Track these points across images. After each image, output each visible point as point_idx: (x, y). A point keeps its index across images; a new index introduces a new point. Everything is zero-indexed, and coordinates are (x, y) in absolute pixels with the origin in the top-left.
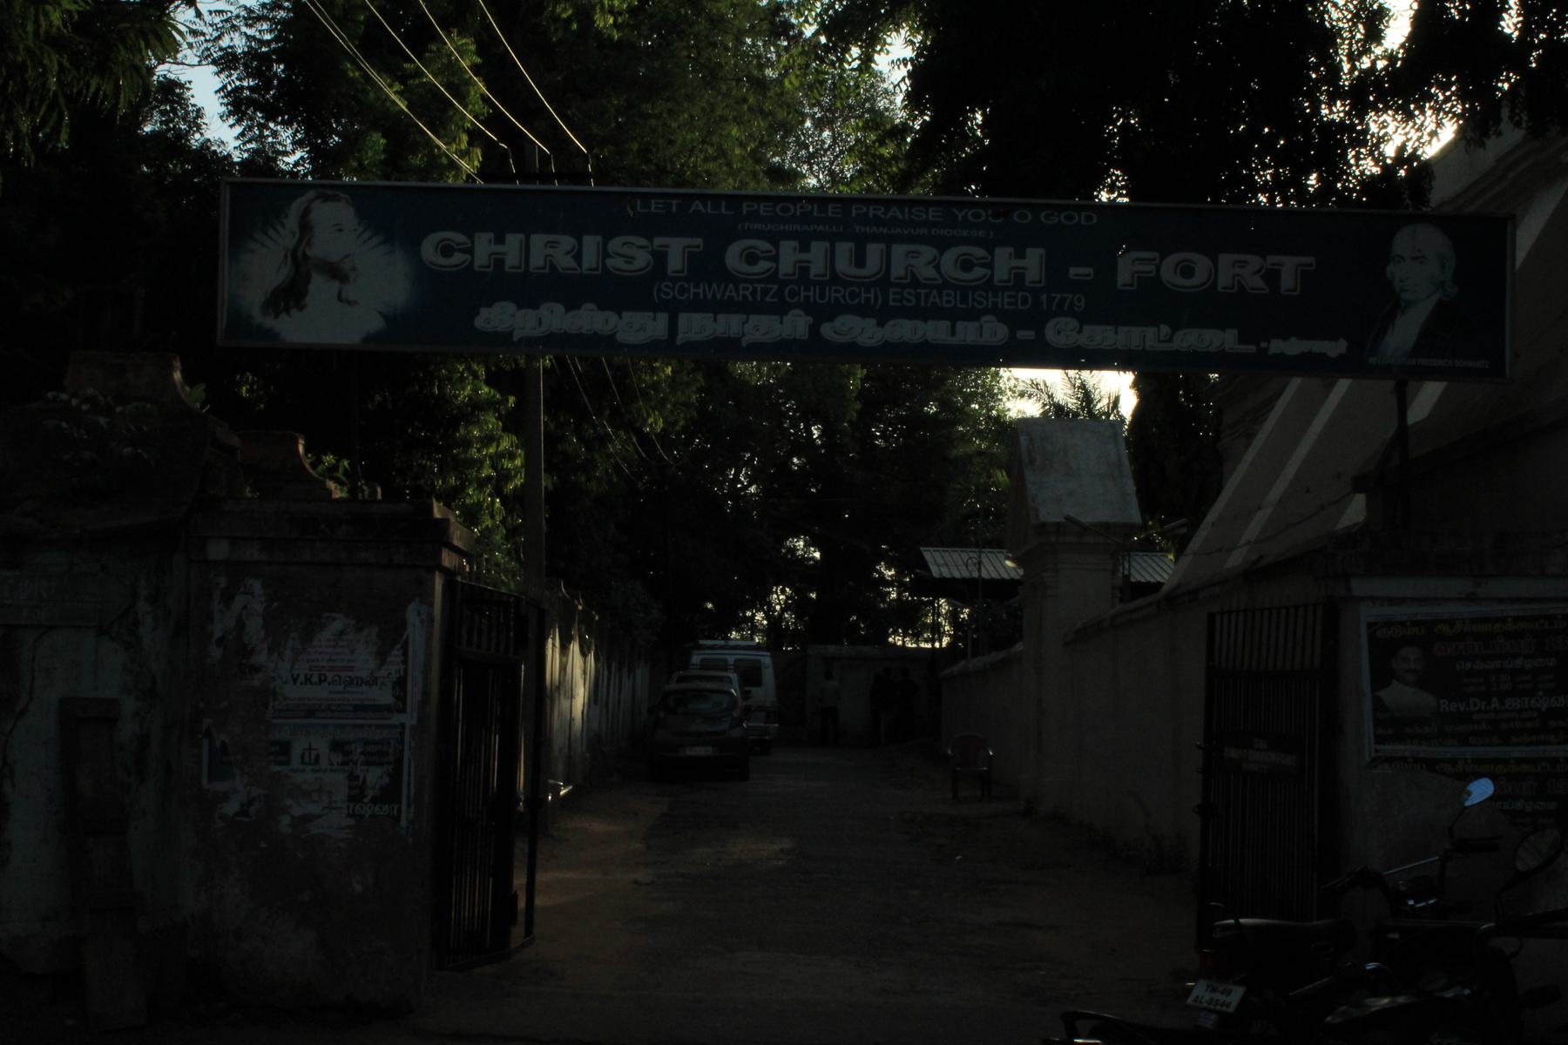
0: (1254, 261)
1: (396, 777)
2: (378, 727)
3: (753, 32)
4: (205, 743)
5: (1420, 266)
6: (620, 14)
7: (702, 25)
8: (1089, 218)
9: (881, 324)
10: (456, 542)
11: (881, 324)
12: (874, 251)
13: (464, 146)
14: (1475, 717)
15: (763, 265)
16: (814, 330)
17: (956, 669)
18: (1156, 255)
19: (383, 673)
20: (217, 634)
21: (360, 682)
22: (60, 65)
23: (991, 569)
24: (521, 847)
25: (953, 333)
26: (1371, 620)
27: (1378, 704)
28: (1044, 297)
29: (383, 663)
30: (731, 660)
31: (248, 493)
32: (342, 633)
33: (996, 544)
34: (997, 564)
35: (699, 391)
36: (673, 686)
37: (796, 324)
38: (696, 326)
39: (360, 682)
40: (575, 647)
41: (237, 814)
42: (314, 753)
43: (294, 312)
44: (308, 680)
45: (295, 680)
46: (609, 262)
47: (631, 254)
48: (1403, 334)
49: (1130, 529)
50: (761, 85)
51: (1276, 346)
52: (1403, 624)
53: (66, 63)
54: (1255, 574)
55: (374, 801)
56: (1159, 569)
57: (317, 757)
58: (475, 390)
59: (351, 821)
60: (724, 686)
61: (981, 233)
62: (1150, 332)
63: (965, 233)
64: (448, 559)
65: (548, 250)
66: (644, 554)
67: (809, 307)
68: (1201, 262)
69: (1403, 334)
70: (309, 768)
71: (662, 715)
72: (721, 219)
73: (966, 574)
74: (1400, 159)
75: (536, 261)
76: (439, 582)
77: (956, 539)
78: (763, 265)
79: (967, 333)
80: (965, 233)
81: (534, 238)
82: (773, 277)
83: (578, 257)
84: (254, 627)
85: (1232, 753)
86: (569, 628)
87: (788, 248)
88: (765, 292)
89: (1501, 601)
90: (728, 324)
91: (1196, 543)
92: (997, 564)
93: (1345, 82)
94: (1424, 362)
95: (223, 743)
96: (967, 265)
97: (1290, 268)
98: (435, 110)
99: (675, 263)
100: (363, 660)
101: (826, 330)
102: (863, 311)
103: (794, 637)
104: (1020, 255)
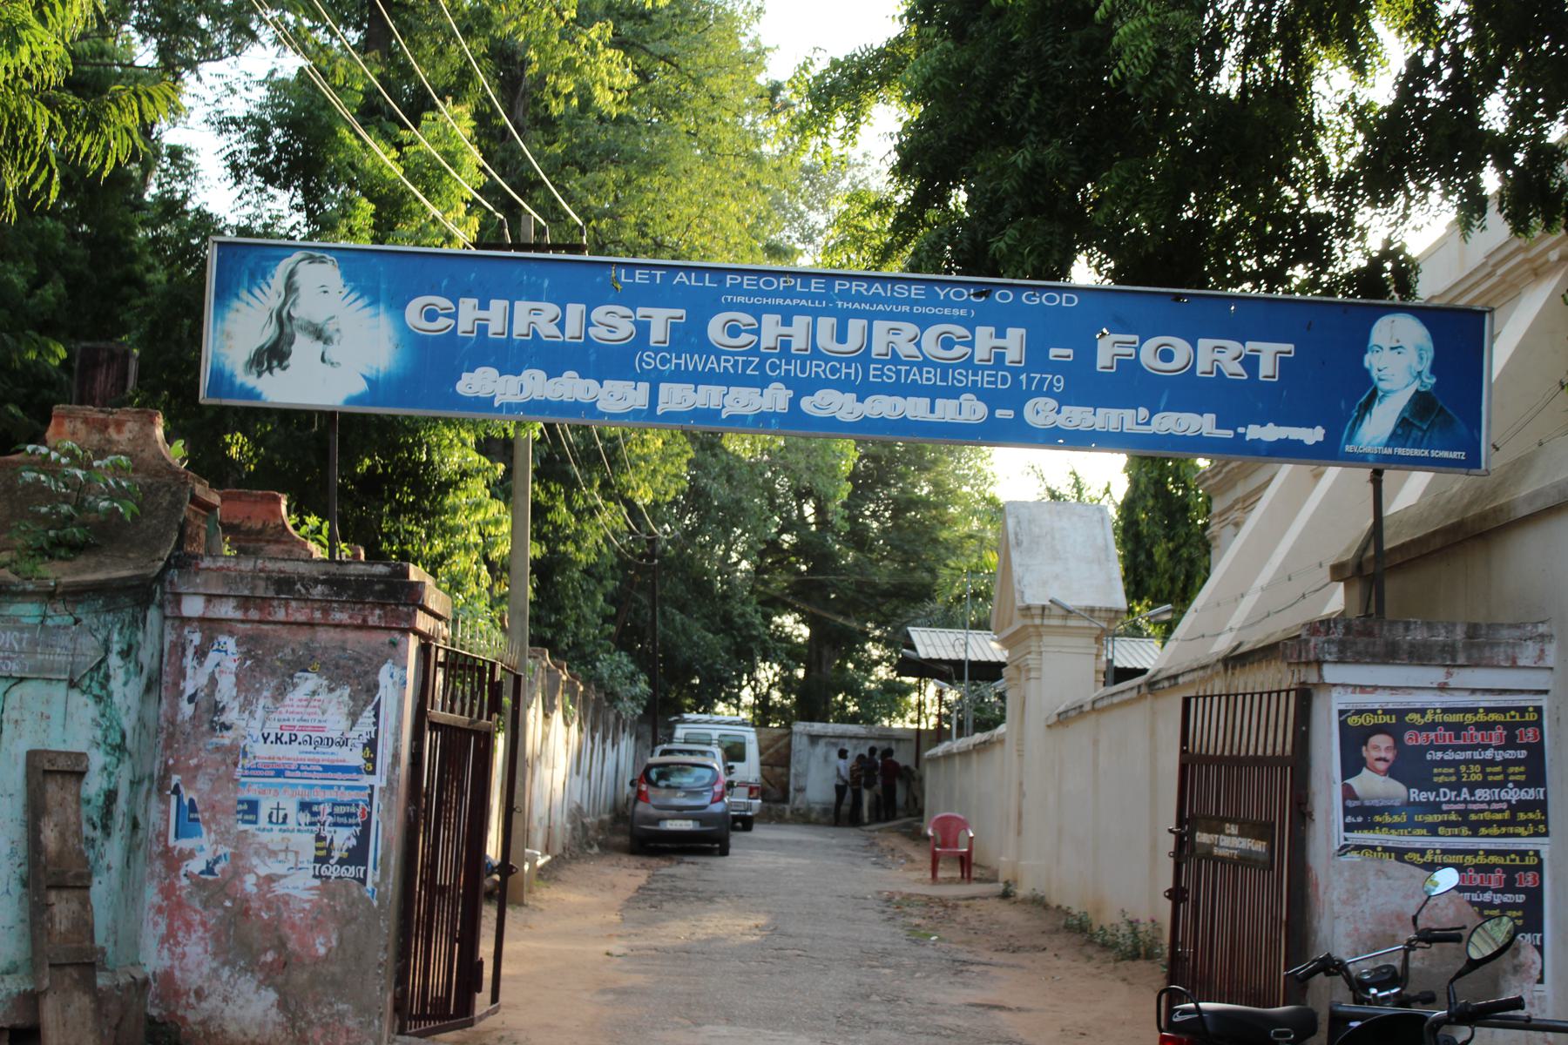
0: (1234, 347)
1: (363, 838)
2: (348, 788)
3: (752, 107)
4: (174, 799)
5: (1398, 356)
6: (620, 91)
7: (702, 102)
8: (1070, 300)
9: (861, 399)
10: (431, 605)
11: (861, 399)
12: (856, 327)
13: (461, 214)
14: (1445, 807)
15: (745, 338)
16: (794, 403)
17: (940, 749)
18: (1135, 338)
19: (353, 734)
20: (189, 691)
21: (330, 742)
22: (52, 122)
23: (977, 650)
24: (489, 914)
25: (932, 411)
26: (1343, 707)
27: (1348, 793)
28: (1023, 377)
29: (353, 724)
30: (715, 735)
31: (226, 550)
32: (314, 693)
33: (982, 625)
34: (984, 645)
35: (690, 462)
36: (657, 759)
37: (776, 398)
38: (676, 397)
39: (330, 742)
40: (557, 716)
41: (202, 873)
42: (282, 813)
43: (277, 371)
44: (278, 739)
45: (265, 739)
46: (591, 331)
47: (613, 324)
48: (1377, 427)
49: (1114, 614)
50: (756, 160)
51: (1253, 432)
52: (1374, 712)
53: (58, 119)
54: (1236, 660)
55: (341, 862)
56: (1128, 653)
57: (285, 816)
58: (464, 458)
59: (317, 882)
60: (709, 762)
61: (963, 312)
62: (1129, 414)
63: (947, 311)
64: (423, 622)
65: (533, 317)
66: (643, 628)
67: (788, 381)
68: (1181, 348)
69: (1377, 427)
70: (276, 828)
71: (644, 787)
72: (706, 289)
73: (953, 656)
74: (1386, 254)
75: (520, 328)
76: (413, 643)
78: (745, 338)
79: (946, 410)
80: (947, 311)
81: (517, 304)
82: (755, 350)
83: (561, 326)
84: (227, 685)
85: (1203, 838)
86: (552, 698)
87: (770, 322)
88: (746, 364)
89: (1474, 691)
90: (708, 396)
91: (1179, 632)
92: (984, 645)
93: (1333, 171)
94: (1401, 451)
95: (192, 801)
96: (947, 344)
97: (1270, 355)
98: (429, 177)
99: (658, 333)
100: (334, 720)
101: (806, 404)
102: (843, 386)
103: (782, 711)
104: (1001, 334)
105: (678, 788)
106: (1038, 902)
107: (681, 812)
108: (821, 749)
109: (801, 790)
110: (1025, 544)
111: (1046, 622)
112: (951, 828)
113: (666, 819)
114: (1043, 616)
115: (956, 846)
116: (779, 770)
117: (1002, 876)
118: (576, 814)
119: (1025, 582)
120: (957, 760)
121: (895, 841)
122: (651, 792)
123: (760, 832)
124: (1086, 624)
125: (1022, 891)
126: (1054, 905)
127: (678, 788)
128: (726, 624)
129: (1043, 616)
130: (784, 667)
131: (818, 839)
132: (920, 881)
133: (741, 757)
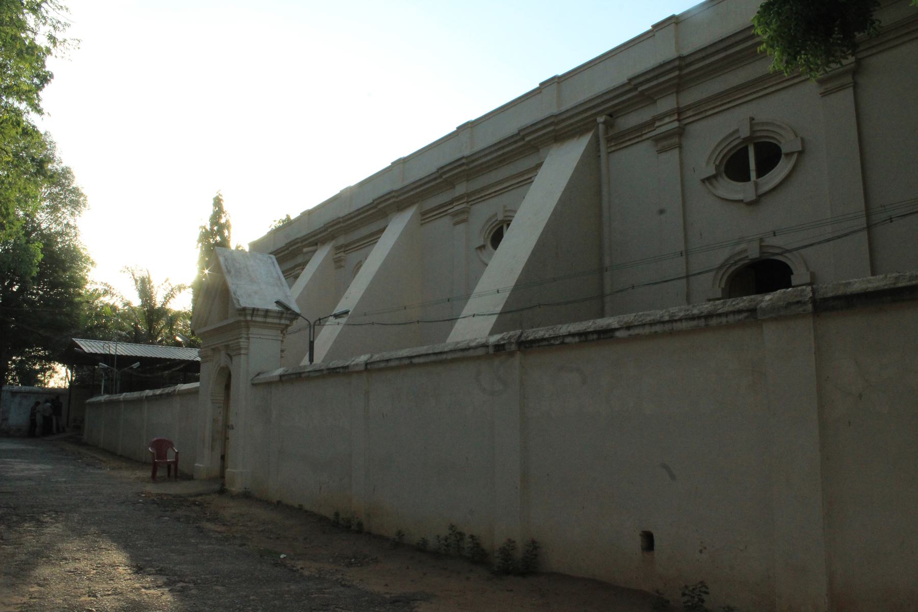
77: (89, 334)
108: (17, 399)
111: (254, 319)
114: (252, 315)
119: (238, 293)
124: (276, 321)
125: (236, 487)
129: (252, 315)
131: (23, 447)
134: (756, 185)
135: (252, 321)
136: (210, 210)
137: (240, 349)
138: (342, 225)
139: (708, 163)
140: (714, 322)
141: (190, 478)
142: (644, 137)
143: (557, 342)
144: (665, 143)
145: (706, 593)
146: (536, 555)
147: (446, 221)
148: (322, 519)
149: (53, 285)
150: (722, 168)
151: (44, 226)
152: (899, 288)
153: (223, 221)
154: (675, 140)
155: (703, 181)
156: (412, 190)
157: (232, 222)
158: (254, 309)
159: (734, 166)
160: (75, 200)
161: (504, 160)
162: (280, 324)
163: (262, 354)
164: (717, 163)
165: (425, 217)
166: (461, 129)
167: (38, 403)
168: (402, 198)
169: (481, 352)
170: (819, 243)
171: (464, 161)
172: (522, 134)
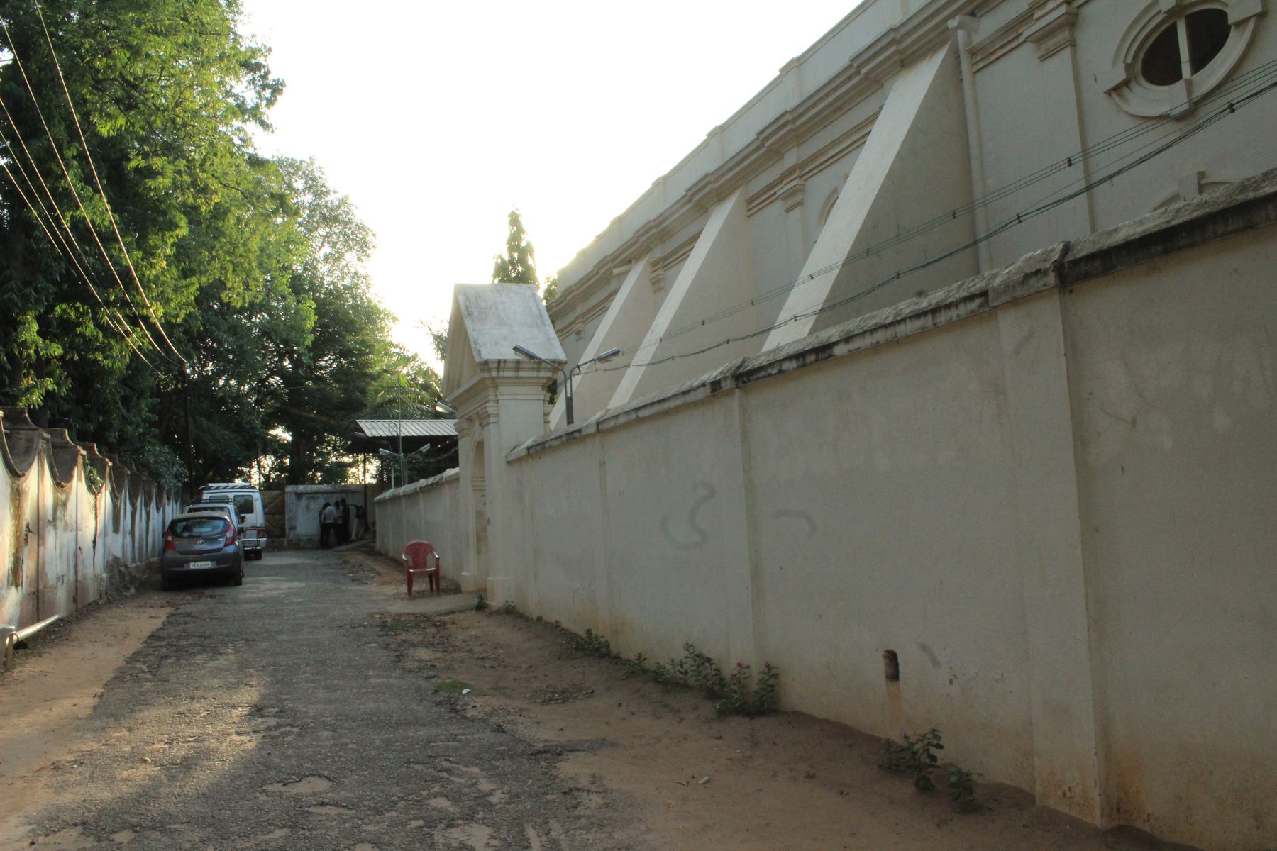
30: (231, 496)
71: (170, 538)
77: (380, 412)
105: (199, 537)
106: (510, 612)
107: (201, 556)
108: (304, 502)
109: (293, 528)
110: (475, 314)
111: (501, 374)
112: (419, 552)
113: (189, 562)
114: (498, 369)
115: (425, 566)
116: (277, 517)
117: (468, 586)
118: (114, 565)
119: (480, 342)
120: (403, 500)
121: (358, 558)
122: (177, 542)
123: (269, 560)
124: (535, 374)
125: (496, 602)
126: (535, 618)
127: (199, 537)
128: (239, 428)
129: (498, 369)
130: (277, 458)
131: (306, 561)
132: (397, 597)
133: (251, 510)
134: (1189, 84)
135: (498, 377)
136: (506, 232)
137: (488, 416)
138: (655, 231)
139: (1115, 62)
140: (942, 318)
141: (456, 589)
142: (1021, 39)
143: (775, 371)
144: (1051, 43)
145: (939, 747)
146: (773, 686)
147: (778, 207)
148: (573, 637)
149: (346, 354)
150: (1139, 66)
151: (327, 280)
152: (1173, 227)
153: (523, 244)
154: (1065, 34)
155: (1109, 93)
156: (731, 169)
157: (535, 246)
158: (499, 362)
159: (1157, 62)
160: (357, 239)
161: (840, 108)
162: (538, 378)
163: (519, 417)
164: (1129, 60)
165: (754, 204)
166: (786, 70)
167: (326, 505)
168: (721, 182)
169: (700, 394)
170: (1130, 167)
171: (788, 117)
172: (855, 65)
